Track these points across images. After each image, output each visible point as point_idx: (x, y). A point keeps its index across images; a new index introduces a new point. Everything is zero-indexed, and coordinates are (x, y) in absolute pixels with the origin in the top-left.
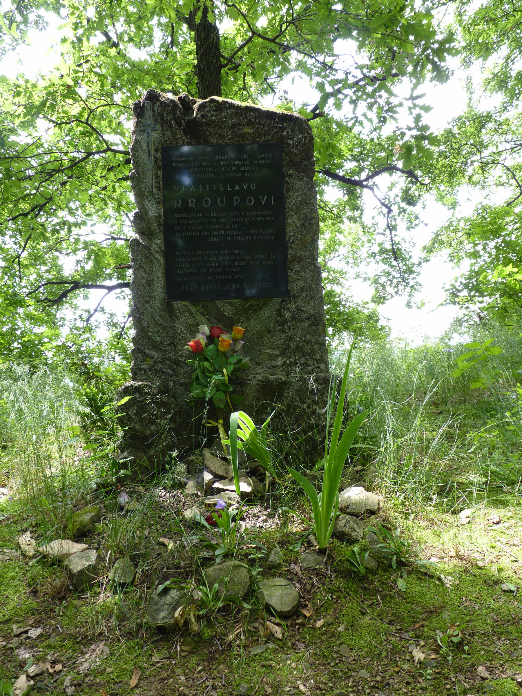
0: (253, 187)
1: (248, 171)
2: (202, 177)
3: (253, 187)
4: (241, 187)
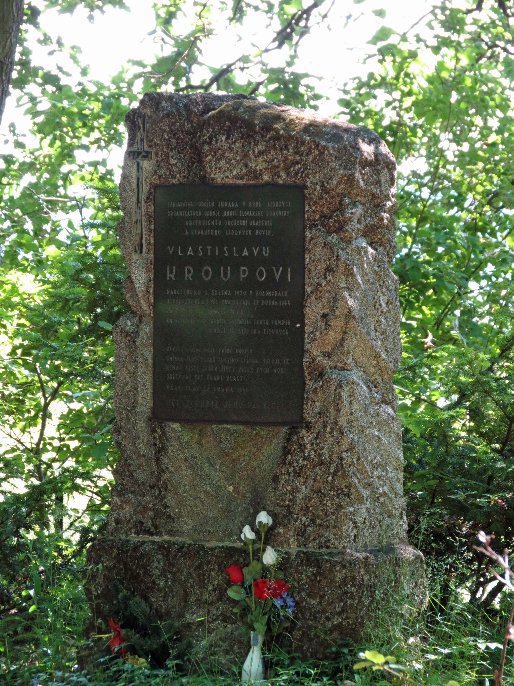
0: (266, 253)
1: (260, 228)
2: (202, 233)
3: (266, 253)
4: (251, 252)
